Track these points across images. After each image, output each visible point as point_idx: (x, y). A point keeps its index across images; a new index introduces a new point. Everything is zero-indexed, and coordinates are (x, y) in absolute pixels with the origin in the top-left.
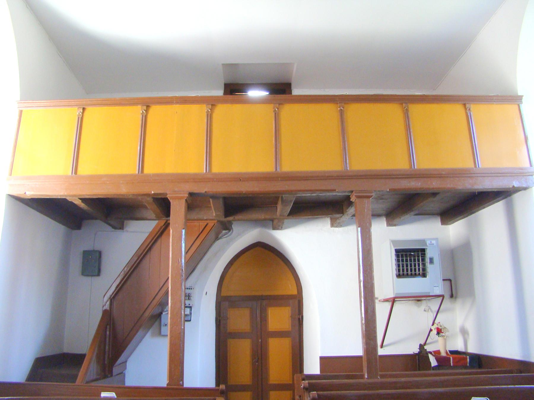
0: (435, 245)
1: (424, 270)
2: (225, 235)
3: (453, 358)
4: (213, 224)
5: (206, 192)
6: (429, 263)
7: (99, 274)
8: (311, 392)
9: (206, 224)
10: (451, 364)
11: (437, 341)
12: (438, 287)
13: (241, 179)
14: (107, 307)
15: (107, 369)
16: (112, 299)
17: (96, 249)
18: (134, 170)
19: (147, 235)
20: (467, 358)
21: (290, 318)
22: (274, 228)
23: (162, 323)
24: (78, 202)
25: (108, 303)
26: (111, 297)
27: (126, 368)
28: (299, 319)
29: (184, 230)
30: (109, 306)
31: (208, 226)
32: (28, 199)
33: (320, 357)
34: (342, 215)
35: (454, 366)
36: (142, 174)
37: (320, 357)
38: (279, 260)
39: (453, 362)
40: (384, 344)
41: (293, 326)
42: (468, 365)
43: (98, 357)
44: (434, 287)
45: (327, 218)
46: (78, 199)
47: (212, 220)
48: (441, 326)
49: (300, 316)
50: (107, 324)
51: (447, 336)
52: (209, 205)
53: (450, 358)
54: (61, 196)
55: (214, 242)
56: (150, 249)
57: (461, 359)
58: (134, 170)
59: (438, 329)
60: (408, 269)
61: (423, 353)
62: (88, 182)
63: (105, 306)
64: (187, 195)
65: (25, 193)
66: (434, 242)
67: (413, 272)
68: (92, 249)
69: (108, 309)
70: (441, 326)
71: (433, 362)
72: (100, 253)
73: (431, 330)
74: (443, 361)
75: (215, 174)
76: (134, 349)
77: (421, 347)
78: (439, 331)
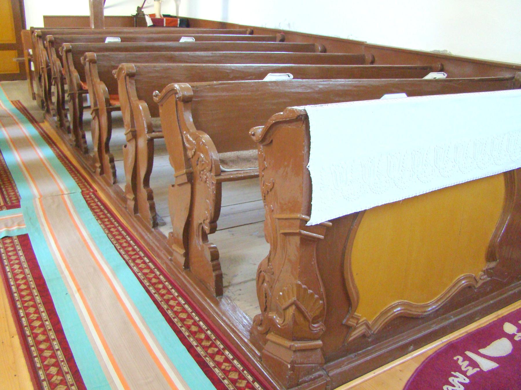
3: (166, 20)
8: (81, 63)
11: (152, 6)
52: (137, 69)
57: (172, 21)
61: (140, 14)
71: (149, 22)
74: (157, 22)
77: (139, 9)
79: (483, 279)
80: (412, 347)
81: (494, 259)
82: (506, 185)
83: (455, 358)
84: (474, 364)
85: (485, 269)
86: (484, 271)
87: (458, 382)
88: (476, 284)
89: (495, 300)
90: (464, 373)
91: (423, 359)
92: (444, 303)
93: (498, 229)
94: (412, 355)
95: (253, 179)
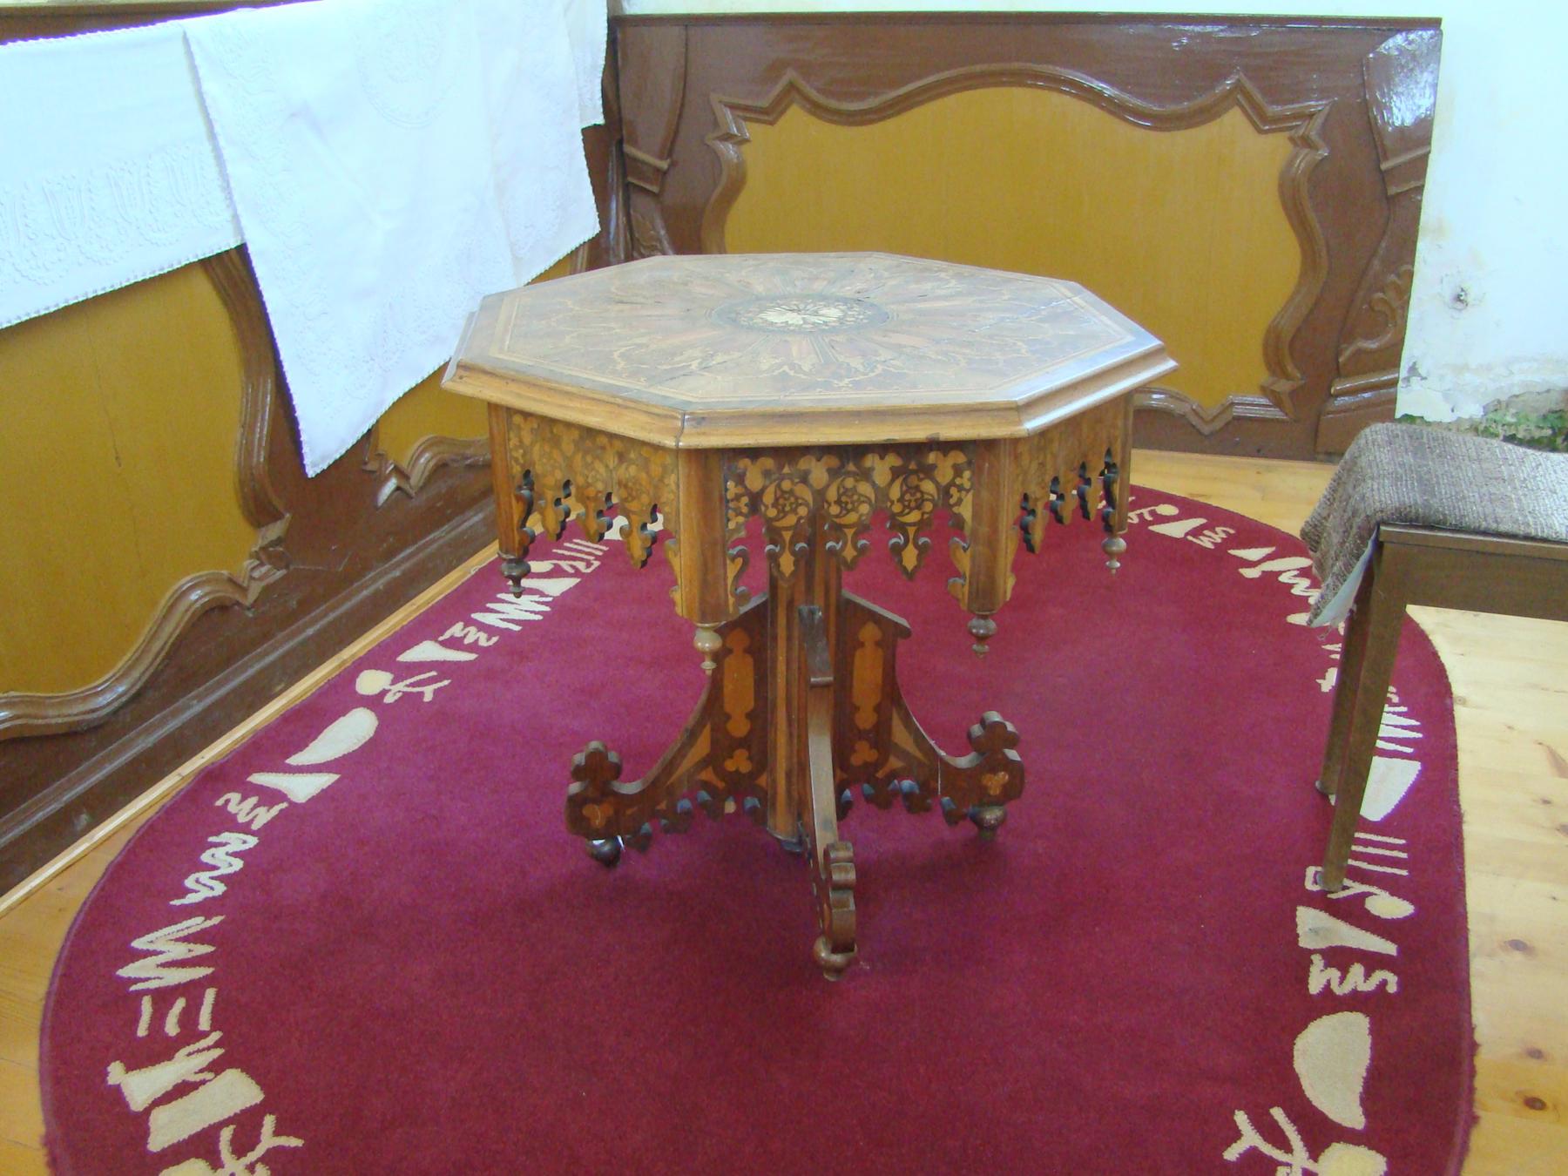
79: (261, 579)
80: (84, 819)
81: (276, 516)
82: (225, 303)
83: (220, 803)
84: (270, 796)
85: (256, 549)
86: (256, 556)
87: (227, 854)
88: (246, 596)
89: (317, 627)
90: (245, 829)
91: (125, 838)
92: (151, 670)
93: (248, 427)
94: (93, 837)
95: (73, 919)
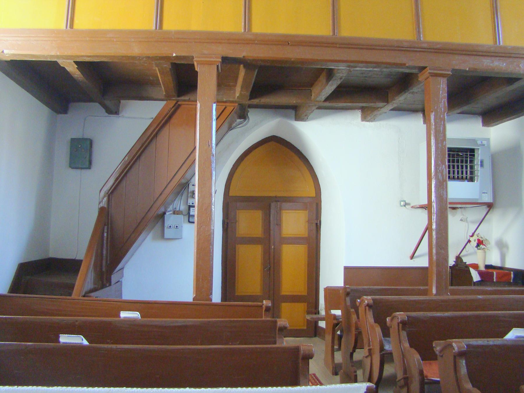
0: (486, 146)
1: (472, 173)
2: (239, 124)
3: (497, 274)
4: (233, 108)
5: (244, 57)
6: (479, 166)
7: (89, 167)
9: (224, 107)
10: (494, 279)
12: (487, 193)
13: (289, 42)
14: (104, 203)
15: (105, 277)
16: (110, 194)
17: (85, 137)
18: (149, 24)
19: (149, 122)
20: (511, 274)
21: (307, 224)
22: (298, 118)
23: (166, 225)
24: (72, 69)
25: (105, 199)
26: (108, 193)
27: (123, 276)
28: (317, 224)
29: (215, 104)
30: (106, 203)
31: (226, 109)
32: (6, 62)
33: (344, 266)
34: (386, 104)
35: (497, 282)
36: (160, 31)
37: (344, 266)
38: (296, 158)
39: (496, 278)
40: (415, 255)
41: (310, 231)
42: (512, 281)
43: (95, 265)
44: (483, 193)
45: (357, 110)
46: (74, 64)
47: (232, 102)
48: (482, 238)
49: (318, 221)
50: (105, 225)
51: (486, 250)
53: (493, 273)
54: (52, 56)
55: (227, 132)
56: (156, 135)
58: (149, 24)
59: (479, 240)
60: (454, 171)
62: (88, 39)
63: (101, 203)
64: (220, 60)
65: (3, 52)
66: (484, 142)
67: (460, 175)
68: (81, 137)
69: (106, 206)
70: (482, 238)
72: (91, 142)
73: (469, 241)
75: (256, 35)
76: (133, 255)
78: (480, 243)
